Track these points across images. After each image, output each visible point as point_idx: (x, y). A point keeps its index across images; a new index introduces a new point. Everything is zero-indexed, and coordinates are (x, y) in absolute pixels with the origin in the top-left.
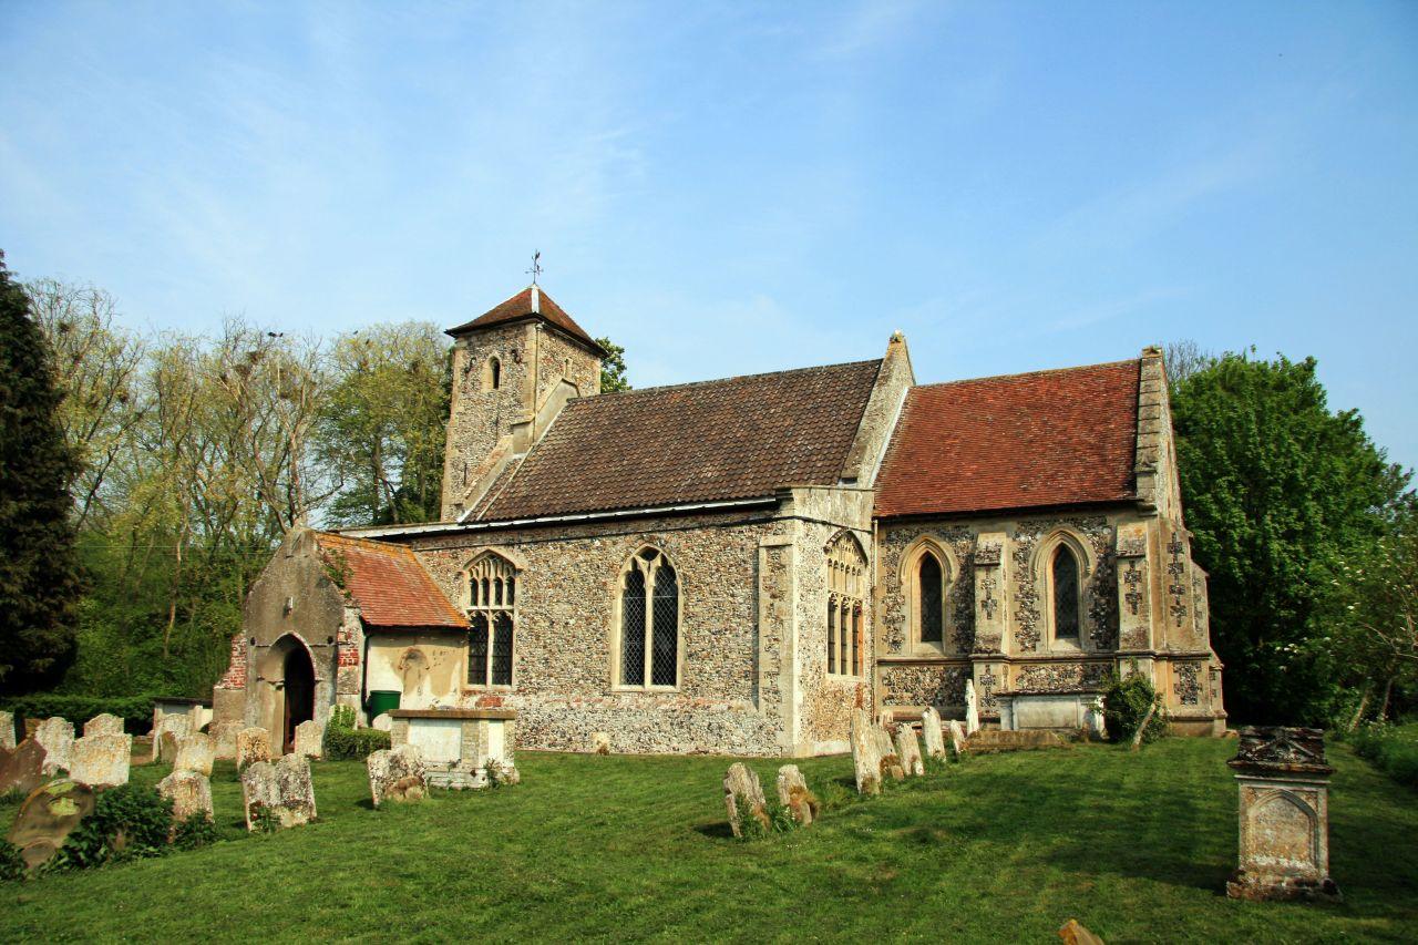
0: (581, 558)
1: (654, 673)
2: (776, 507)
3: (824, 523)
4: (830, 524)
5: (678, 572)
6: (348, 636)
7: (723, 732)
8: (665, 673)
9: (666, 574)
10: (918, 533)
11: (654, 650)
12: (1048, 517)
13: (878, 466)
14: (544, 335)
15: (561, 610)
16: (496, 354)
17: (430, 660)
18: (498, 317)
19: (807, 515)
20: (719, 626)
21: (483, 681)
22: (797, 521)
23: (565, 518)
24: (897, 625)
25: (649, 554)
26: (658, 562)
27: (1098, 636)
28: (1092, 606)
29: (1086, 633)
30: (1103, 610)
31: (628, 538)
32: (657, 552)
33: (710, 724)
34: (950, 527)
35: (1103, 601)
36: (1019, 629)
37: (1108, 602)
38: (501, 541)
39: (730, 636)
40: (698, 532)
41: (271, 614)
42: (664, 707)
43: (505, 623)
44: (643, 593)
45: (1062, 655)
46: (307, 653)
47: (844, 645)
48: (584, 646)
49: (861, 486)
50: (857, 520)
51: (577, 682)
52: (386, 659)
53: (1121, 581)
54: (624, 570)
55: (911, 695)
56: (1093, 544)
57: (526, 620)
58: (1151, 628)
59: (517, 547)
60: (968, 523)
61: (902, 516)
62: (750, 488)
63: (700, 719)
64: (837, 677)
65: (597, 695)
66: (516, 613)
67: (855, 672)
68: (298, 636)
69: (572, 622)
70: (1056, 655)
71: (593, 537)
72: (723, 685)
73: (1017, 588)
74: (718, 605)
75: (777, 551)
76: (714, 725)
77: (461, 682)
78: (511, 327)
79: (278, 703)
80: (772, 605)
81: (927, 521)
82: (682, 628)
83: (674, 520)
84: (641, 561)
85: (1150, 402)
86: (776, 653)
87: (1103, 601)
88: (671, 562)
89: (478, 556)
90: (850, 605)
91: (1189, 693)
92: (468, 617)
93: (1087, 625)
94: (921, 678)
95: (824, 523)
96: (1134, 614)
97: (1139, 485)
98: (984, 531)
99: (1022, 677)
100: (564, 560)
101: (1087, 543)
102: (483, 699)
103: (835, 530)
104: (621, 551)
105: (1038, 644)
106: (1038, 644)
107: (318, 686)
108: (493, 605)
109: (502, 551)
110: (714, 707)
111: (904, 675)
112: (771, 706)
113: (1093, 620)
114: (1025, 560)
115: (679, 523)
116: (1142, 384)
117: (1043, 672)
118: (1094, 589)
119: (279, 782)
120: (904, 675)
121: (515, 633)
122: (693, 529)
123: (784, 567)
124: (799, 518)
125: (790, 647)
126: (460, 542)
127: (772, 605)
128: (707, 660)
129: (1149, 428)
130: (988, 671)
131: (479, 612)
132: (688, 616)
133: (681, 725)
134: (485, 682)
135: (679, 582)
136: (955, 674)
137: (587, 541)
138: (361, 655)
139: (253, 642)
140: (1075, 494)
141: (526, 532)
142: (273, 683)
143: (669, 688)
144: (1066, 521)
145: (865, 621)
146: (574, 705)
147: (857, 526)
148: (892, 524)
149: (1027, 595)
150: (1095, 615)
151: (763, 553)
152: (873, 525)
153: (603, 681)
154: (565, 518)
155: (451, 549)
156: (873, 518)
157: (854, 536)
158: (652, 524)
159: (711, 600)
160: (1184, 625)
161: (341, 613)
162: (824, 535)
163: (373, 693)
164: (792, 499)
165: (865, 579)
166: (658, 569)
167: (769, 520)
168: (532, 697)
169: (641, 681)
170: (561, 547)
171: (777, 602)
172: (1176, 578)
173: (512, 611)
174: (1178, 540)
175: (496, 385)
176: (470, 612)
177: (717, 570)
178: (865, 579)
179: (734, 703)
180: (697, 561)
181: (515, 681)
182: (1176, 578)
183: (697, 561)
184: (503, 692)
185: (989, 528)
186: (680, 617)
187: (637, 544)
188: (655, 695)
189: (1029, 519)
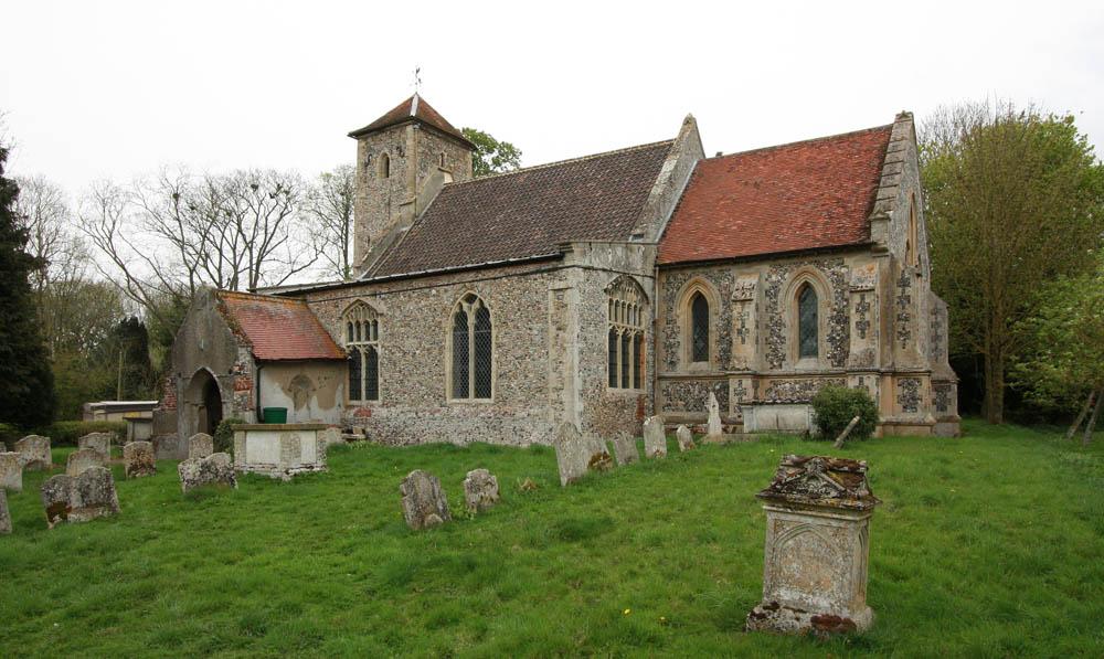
1: (476, 389)
2: (560, 258)
3: (604, 270)
4: (611, 271)
5: (491, 312)
6: (242, 368)
7: (524, 433)
8: (484, 390)
9: (483, 314)
10: (690, 277)
11: (476, 372)
12: (795, 260)
13: (665, 224)
14: (422, 134)
15: (410, 344)
16: (386, 151)
17: (316, 383)
19: (587, 263)
20: (520, 353)
21: (465, 394)
22: (576, 269)
24: (673, 350)
25: (471, 299)
26: (476, 305)
27: (834, 356)
28: (829, 332)
30: (838, 335)
32: (476, 297)
34: (715, 270)
35: (839, 328)
37: (843, 329)
40: (505, 280)
41: (190, 354)
42: (482, 415)
43: (372, 354)
44: (467, 329)
45: (803, 372)
47: (625, 366)
48: (427, 370)
49: (648, 241)
50: (639, 267)
52: (277, 384)
58: (879, 350)
60: (731, 267)
61: (677, 263)
62: (539, 241)
63: (507, 423)
64: (619, 390)
65: (436, 406)
67: (637, 386)
68: (208, 369)
69: (418, 352)
70: (798, 372)
71: (431, 287)
74: (519, 337)
75: (561, 293)
79: (201, 419)
81: (697, 267)
82: (494, 356)
84: (465, 305)
85: (895, 159)
86: (560, 373)
87: (839, 328)
88: (487, 305)
89: (351, 305)
90: (632, 334)
91: (910, 402)
93: (825, 347)
95: (604, 270)
96: (863, 338)
97: (873, 231)
98: (742, 274)
99: (771, 389)
100: (411, 306)
101: (822, 278)
102: (360, 411)
103: (615, 276)
104: (448, 297)
105: (783, 363)
106: (783, 363)
107: (224, 406)
108: (619, 322)
109: (369, 301)
110: (517, 415)
113: (830, 344)
114: (776, 296)
115: (491, 274)
116: (891, 145)
117: (787, 385)
118: (832, 318)
119: (80, 490)
122: (501, 278)
123: (566, 305)
124: (579, 267)
125: (572, 368)
126: (340, 294)
129: (890, 182)
130: (740, 384)
131: (371, 347)
134: (360, 399)
135: (492, 319)
136: (718, 387)
138: (255, 382)
139: (180, 375)
140: (818, 240)
141: (384, 285)
144: (810, 263)
145: (646, 349)
146: (420, 414)
147: (640, 272)
148: (670, 270)
149: (776, 324)
150: (832, 339)
152: (655, 271)
156: (655, 266)
157: (635, 280)
158: (471, 276)
159: (515, 333)
161: (235, 351)
162: (606, 281)
163: (264, 410)
164: (572, 251)
165: (646, 315)
166: (478, 310)
167: (556, 269)
168: (393, 409)
171: (561, 333)
172: (903, 308)
173: (377, 345)
174: (907, 276)
178: (646, 315)
181: (380, 398)
182: (903, 308)
184: (372, 406)
185: (746, 271)
186: (493, 346)
188: (477, 405)
189: (781, 262)
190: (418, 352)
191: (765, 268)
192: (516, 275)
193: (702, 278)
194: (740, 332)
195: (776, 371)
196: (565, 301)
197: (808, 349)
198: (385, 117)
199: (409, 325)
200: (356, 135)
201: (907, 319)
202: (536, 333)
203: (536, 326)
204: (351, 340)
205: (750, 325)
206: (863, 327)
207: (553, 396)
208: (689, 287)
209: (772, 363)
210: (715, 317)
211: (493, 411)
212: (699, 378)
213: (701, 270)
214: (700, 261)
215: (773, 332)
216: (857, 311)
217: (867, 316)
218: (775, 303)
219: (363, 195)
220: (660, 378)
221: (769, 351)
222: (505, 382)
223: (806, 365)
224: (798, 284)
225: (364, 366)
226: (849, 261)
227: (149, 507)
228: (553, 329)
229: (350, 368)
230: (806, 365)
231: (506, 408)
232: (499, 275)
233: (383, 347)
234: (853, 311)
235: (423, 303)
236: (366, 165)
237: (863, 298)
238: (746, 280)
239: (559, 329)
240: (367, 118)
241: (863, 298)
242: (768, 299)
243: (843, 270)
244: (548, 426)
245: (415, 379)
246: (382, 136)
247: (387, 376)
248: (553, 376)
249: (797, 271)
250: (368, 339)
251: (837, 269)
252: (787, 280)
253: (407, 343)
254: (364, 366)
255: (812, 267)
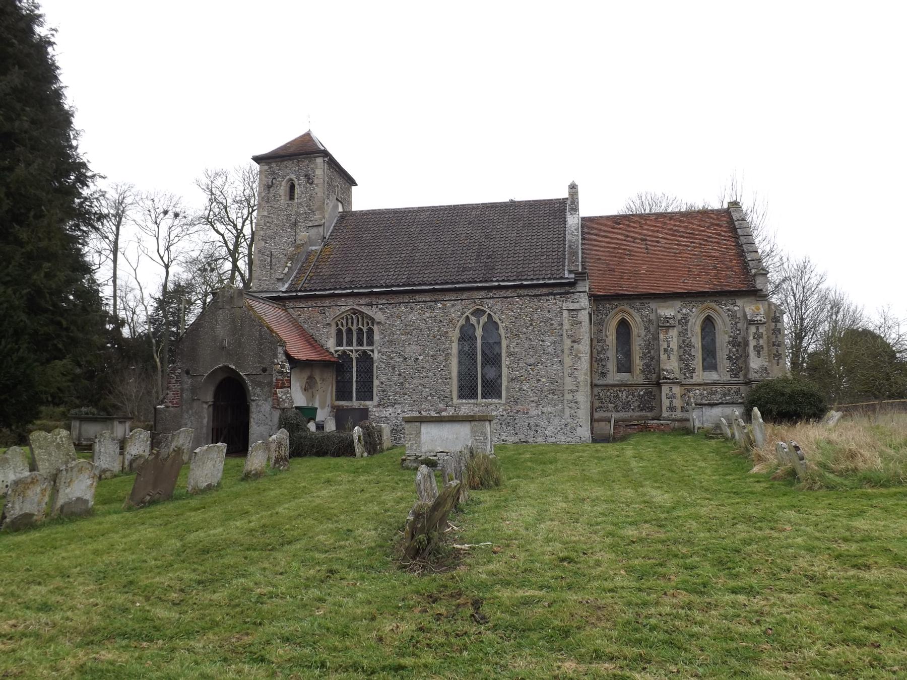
0: (427, 314)
1: (483, 392)
8: (492, 389)
9: (491, 325)
12: (700, 299)
15: (411, 350)
16: (293, 176)
18: (292, 150)
20: (532, 360)
21: (474, 395)
23: (457, 286)
24: (604, 363)
25: (478, 313)
26: (484, 319)
27: (731, 370)
28: (728, 353)
29: (724, 369)
30: (734, 355)
31: (463, 302)
33: (529, 424)
34: (638, 303)
36: (682, 366)
38: (362, 302)
39: (541, 367)
43: (366, 359)
46: (243, 380)
48: (430, 374)
51: (426, 398)
53: (751, 338)
54: (459, 324)
55: (613, 405)
56: (728, 315)
57: (384, 357)
59: (374, 307)
63: (522, 422)
66: (376, 352)
71: (436, 301)
72: (537, 398)
73: (681, 341)
76: (532, 424)
77: (332, 400)
78: (304, 158)
80: (572, 347)
83: (498, 291)
84: (473, 319)
88: (496, 318)
92: (336, 355)
93: (724, 363)
94: (620, 395)
99: (685, 395)
101: (722, 313)
109: (364, 309)
111: (608, 394)
112: (573, 412)
115: (503, 293)
117: (697, 391)
118: (729, 343)
120: (608, 394)
121: (375, 365)
122: (513, 297)
126: (327, 303)
127: (572, 347)
128: (524, 382)
130: (671, 390)
131: (365, 352)
132: (510, 354)
133: (508, 424)
135: (502, 332)
136: (642, 393)
137: (432, 304)
142: (206, 403)
143: (496, 401)
150: (729, 358)
151: (565, 313)
153: (446, 397)
154: (457, 286)
155: (319, 307)
158: (481, 294)
160: (780, 365)
167: (569, 293)
169: (476, 397)
170: (411, 308)
171: (576, 346)
172: (776, 337)
173: (372, 351)
175: (292, 197)
176: (336, 351)
177: (531, 324)
179: (545, 410)
180: (516, 318)
181: (376, 399)
182: (776, 337)
183: (516, 318)
187: (470, 306)
189: (689, 300)
190: (421, 358)
191: (678, 304)
192: (527, 295)
193: (626, 307)
194: (666, 350)
195: (688, 381)
196: (579, 319)
197: (710, 364)
198: (292, 143)
199: (410, 333)
200: (258, 159)
201: (779, 345)
202: (549, 344)
203: (548, 340)
204: (362, 345)
205: (674, 345)
206: (758, 349)
207: (568, 397)
208: (616, 314)
209: (685, 375)
210: (638, 339)
211: (505, 410)
212: (626, 385)
213: (626, 302)
214: (626, 295)
215: (685, 352)
216: (754, 338)
217: (761, 342)
218: (686, 330)
219: (266, 213)
220: (596, 385)
221: (682, 366)
222: (517, 385)
223: (713, 376)
224: (702, 317)
225: (354, 369)
226: (740, 302)
227: (569, 451)
228: (568, 342)
229: (337, 371)
230: (713, 376)
231: (519, 407)
232: (511, 295)
233: (379, 352)
234: (751, 338)
235: (427, 314)
236: (269, 187)
237: (757, 329)
238: (668, 311)
239: (574, 342)
240: (265, 149)
241: (757, 329)
242: (680, 326)
243: (736, 308)
244: (563, 422)
245: (418, 382)
246: (289, 163)
247: (384, 379)
248: (568, 380)
249: (701, 307)
250: (360, 343)
251: (731, 307)
252: (696, 315)
253: (408, 349)
254: (354, 369)
255: (713, 305)
